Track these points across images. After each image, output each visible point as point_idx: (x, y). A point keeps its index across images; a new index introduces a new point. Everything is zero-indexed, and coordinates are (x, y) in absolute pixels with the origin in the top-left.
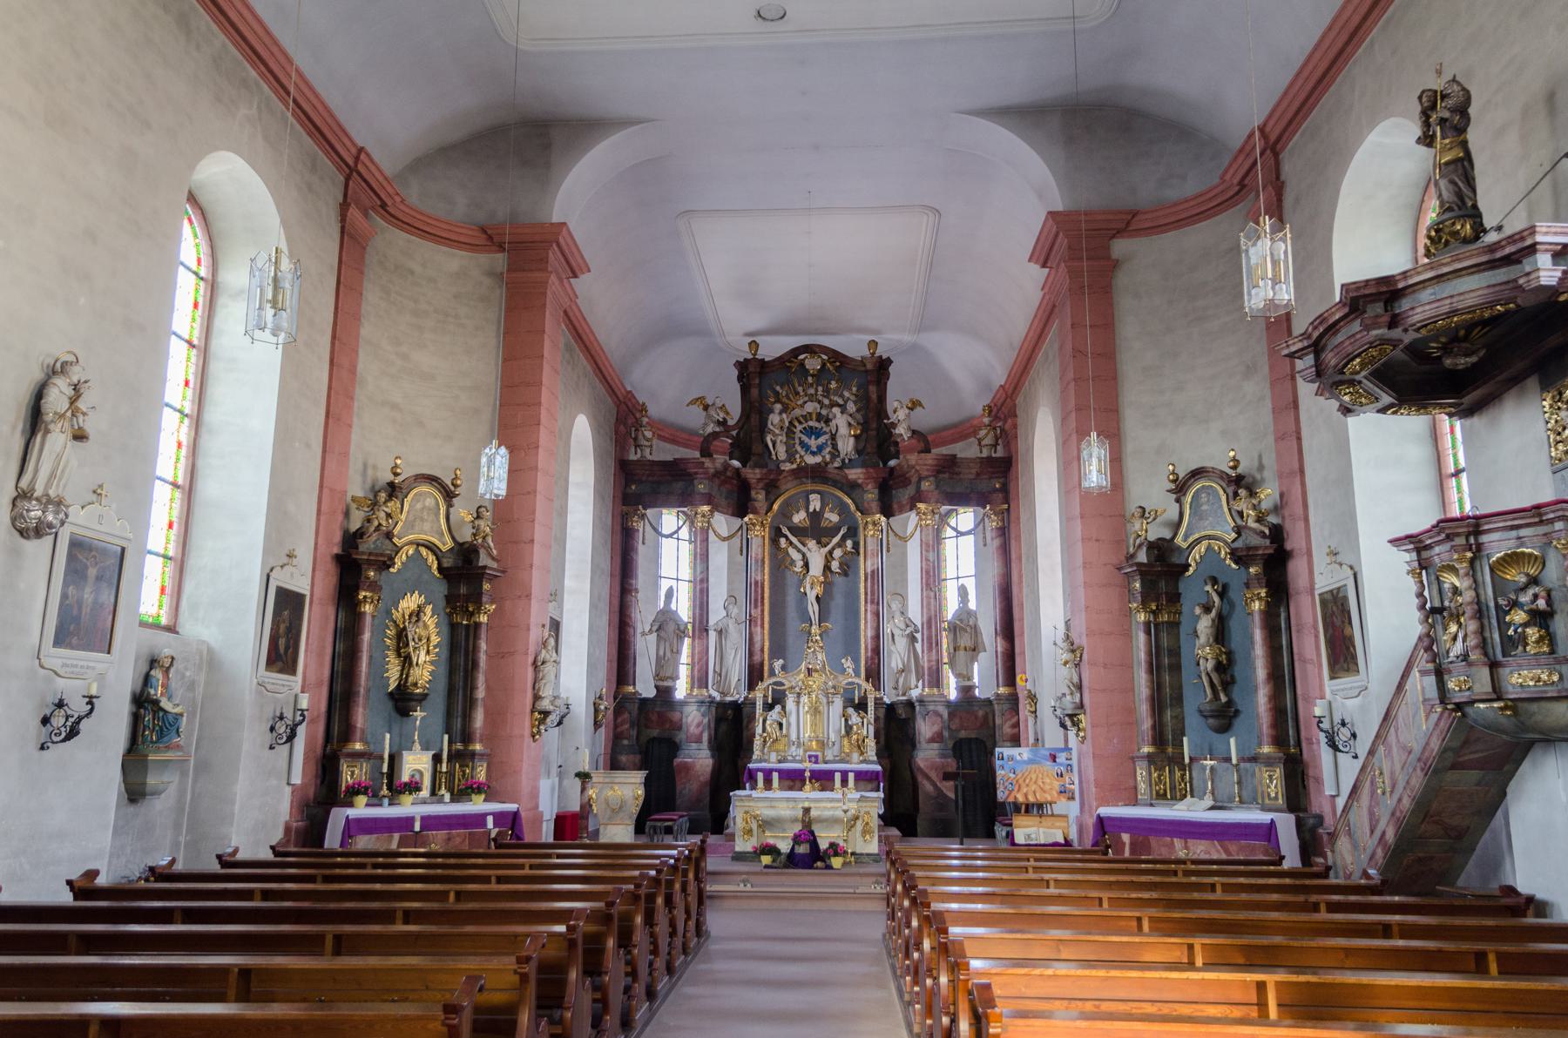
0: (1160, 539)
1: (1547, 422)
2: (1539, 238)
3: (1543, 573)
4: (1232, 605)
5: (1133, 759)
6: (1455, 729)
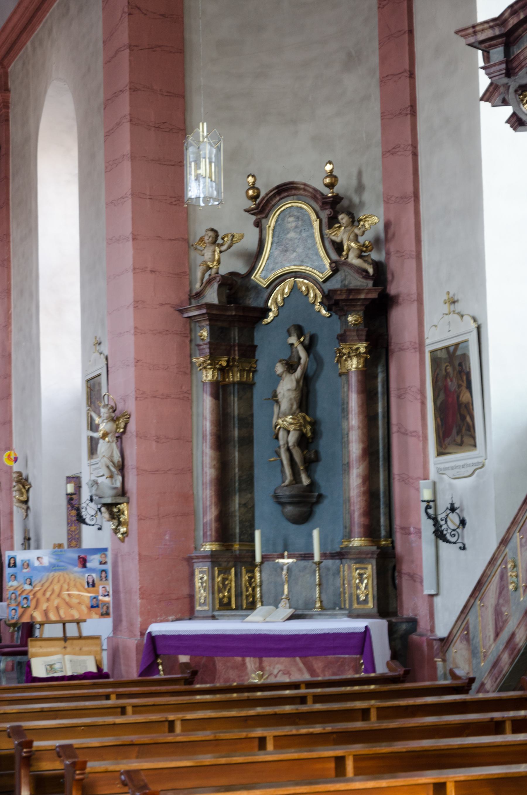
0: (232, 274)
5: (190, 561)
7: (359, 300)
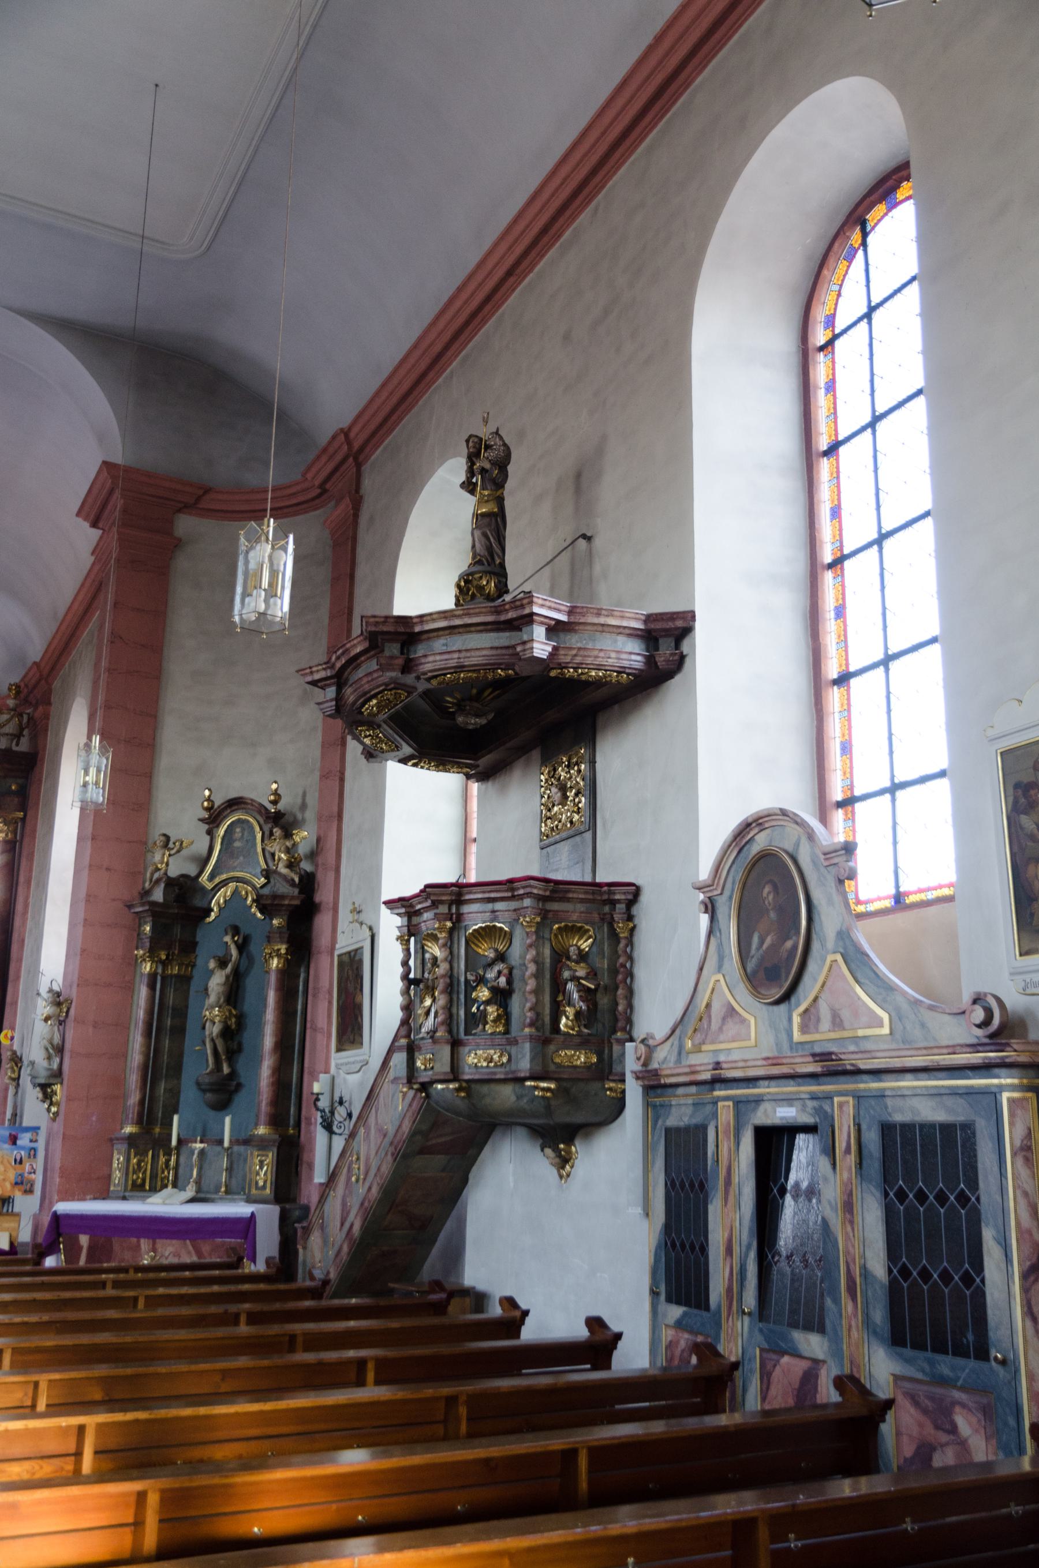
0: (183, 876)
1: (542, 797)
2: (536, 609)
3: (510, 950)
4: (251, 960)
6: (425, 1110)
7: (283, 905)
